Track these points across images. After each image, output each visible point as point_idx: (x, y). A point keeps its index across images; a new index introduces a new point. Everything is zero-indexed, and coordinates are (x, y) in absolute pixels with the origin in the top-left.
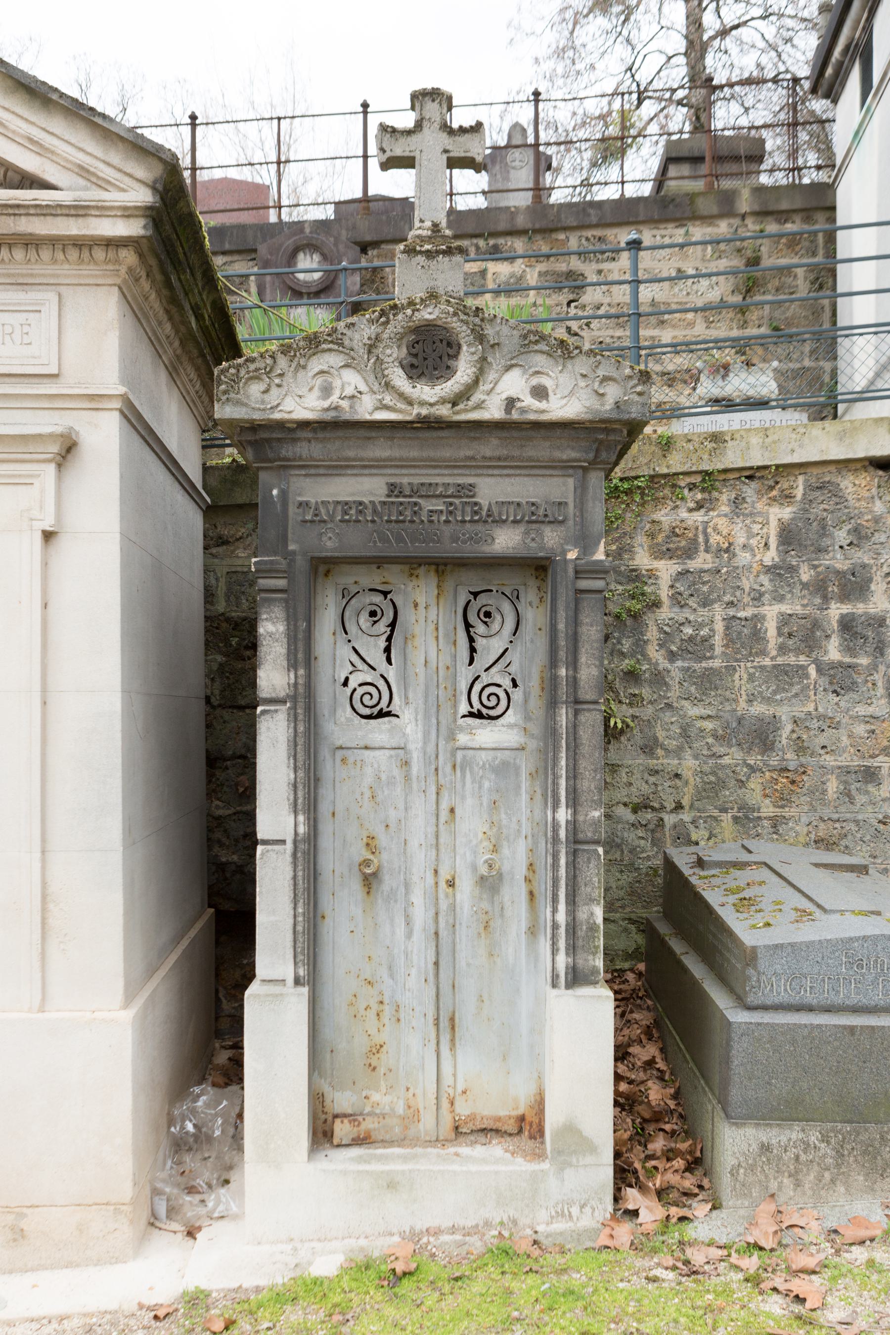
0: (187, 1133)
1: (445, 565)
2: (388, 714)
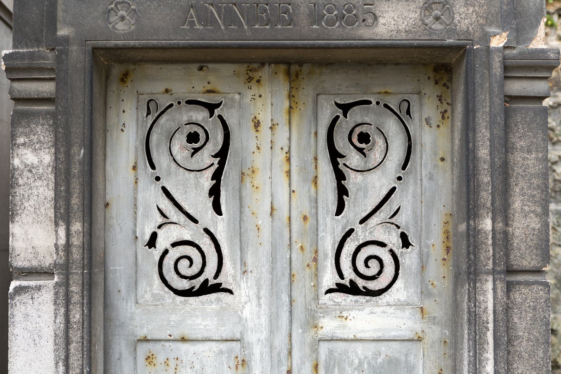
1: (301, 63)
2: (217, 288)
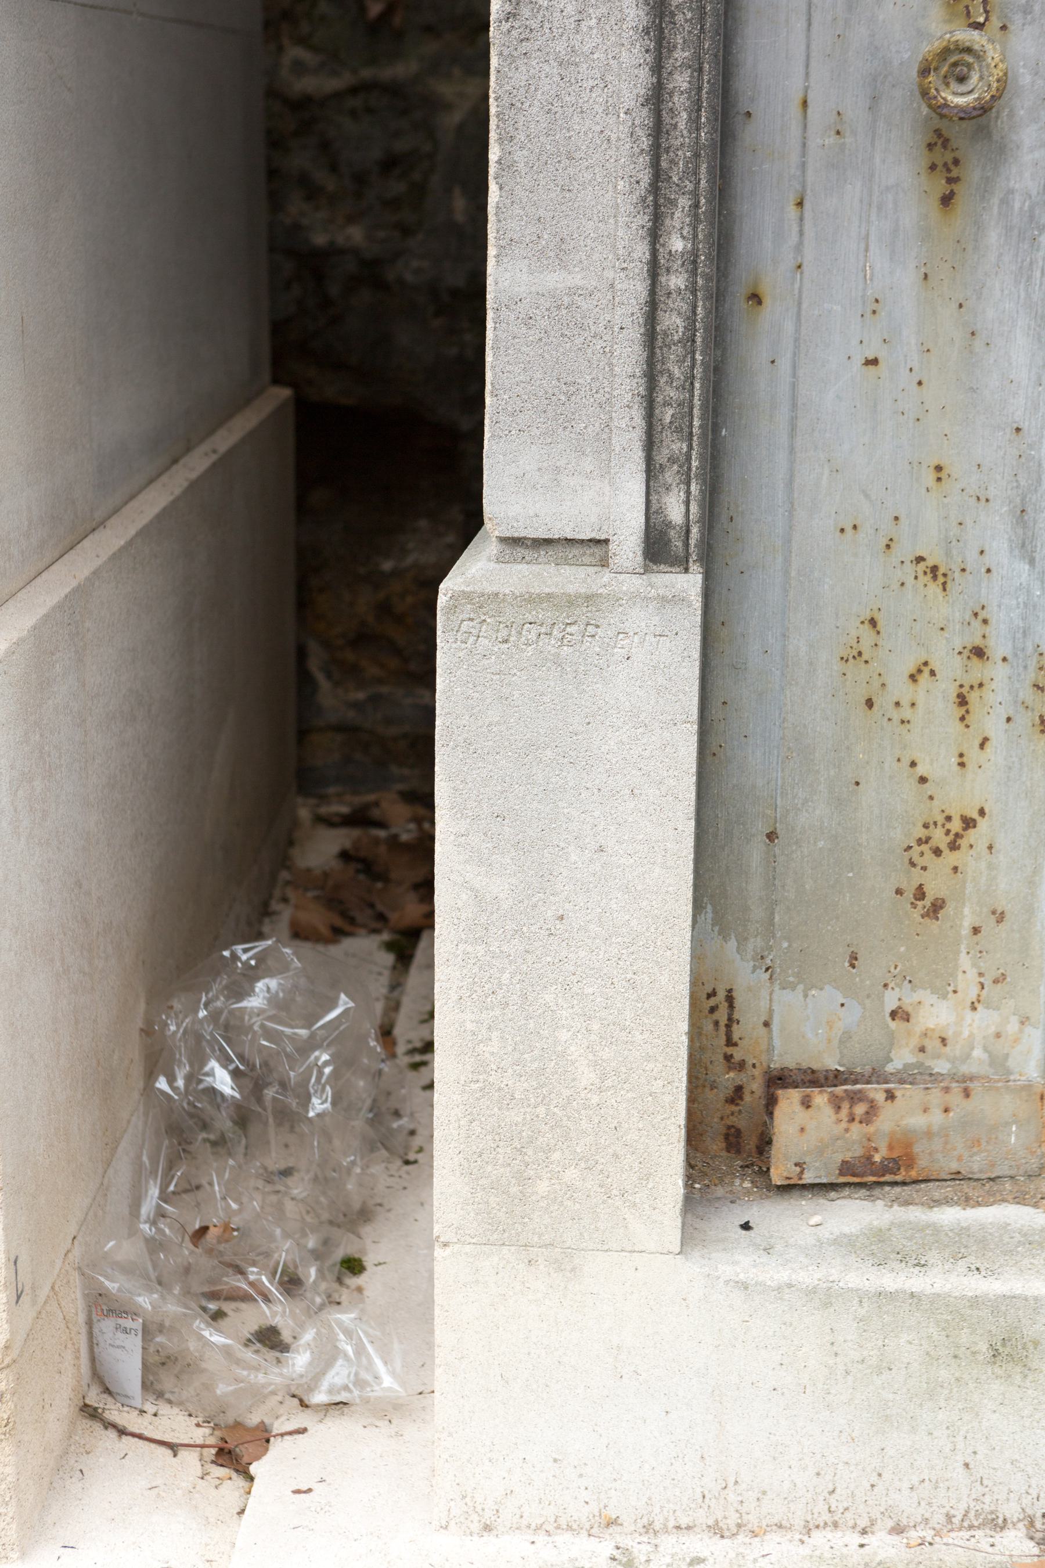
0: (212, 1092)
